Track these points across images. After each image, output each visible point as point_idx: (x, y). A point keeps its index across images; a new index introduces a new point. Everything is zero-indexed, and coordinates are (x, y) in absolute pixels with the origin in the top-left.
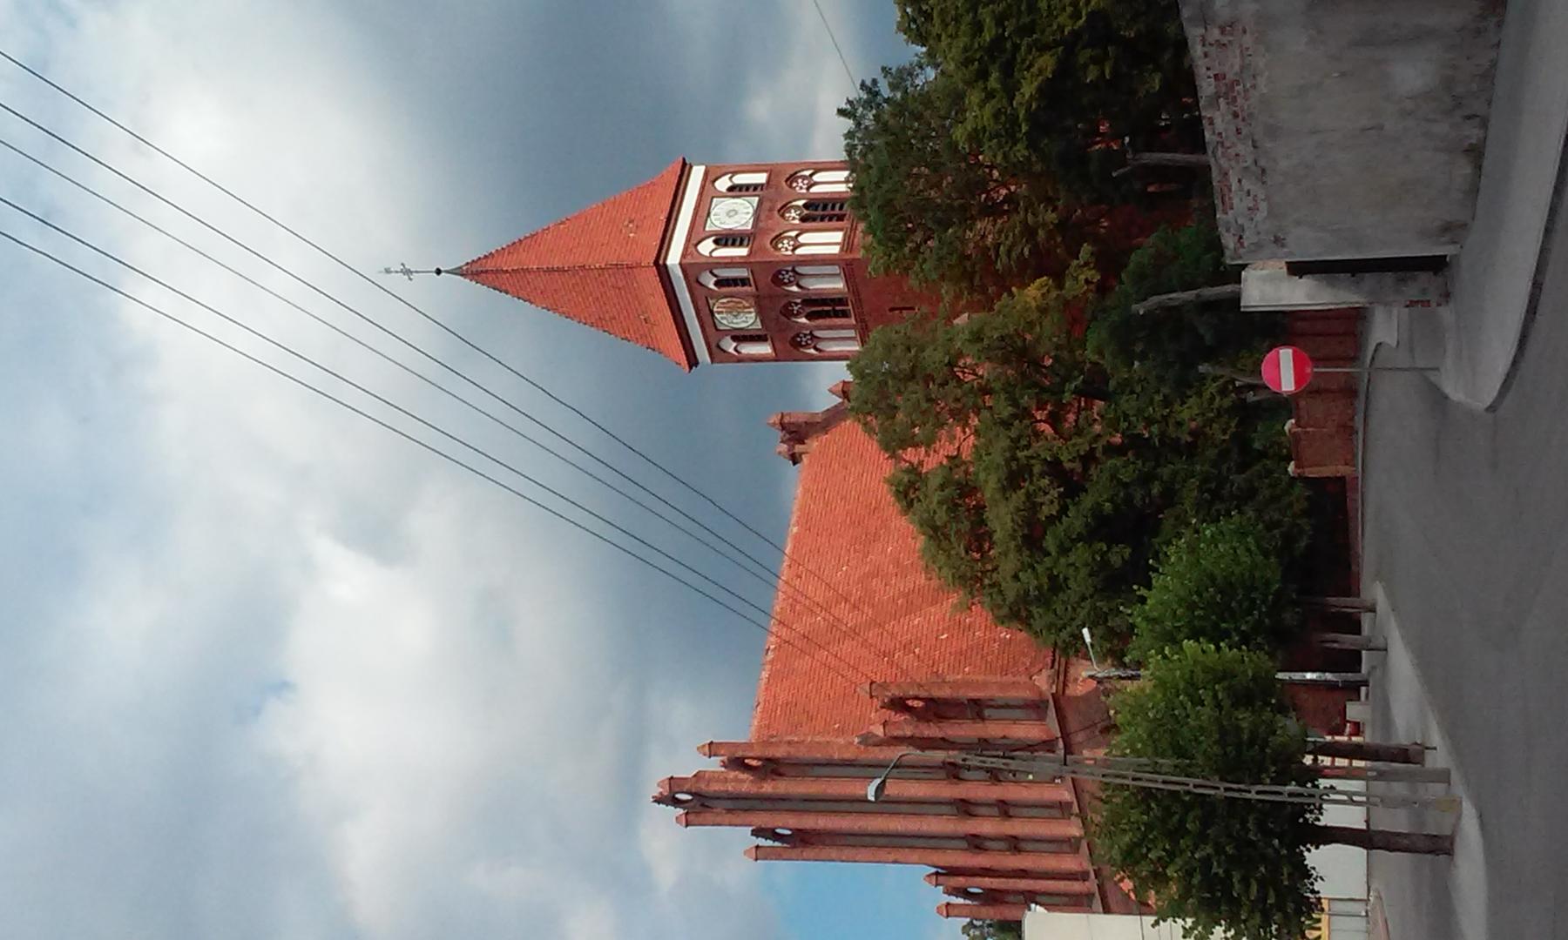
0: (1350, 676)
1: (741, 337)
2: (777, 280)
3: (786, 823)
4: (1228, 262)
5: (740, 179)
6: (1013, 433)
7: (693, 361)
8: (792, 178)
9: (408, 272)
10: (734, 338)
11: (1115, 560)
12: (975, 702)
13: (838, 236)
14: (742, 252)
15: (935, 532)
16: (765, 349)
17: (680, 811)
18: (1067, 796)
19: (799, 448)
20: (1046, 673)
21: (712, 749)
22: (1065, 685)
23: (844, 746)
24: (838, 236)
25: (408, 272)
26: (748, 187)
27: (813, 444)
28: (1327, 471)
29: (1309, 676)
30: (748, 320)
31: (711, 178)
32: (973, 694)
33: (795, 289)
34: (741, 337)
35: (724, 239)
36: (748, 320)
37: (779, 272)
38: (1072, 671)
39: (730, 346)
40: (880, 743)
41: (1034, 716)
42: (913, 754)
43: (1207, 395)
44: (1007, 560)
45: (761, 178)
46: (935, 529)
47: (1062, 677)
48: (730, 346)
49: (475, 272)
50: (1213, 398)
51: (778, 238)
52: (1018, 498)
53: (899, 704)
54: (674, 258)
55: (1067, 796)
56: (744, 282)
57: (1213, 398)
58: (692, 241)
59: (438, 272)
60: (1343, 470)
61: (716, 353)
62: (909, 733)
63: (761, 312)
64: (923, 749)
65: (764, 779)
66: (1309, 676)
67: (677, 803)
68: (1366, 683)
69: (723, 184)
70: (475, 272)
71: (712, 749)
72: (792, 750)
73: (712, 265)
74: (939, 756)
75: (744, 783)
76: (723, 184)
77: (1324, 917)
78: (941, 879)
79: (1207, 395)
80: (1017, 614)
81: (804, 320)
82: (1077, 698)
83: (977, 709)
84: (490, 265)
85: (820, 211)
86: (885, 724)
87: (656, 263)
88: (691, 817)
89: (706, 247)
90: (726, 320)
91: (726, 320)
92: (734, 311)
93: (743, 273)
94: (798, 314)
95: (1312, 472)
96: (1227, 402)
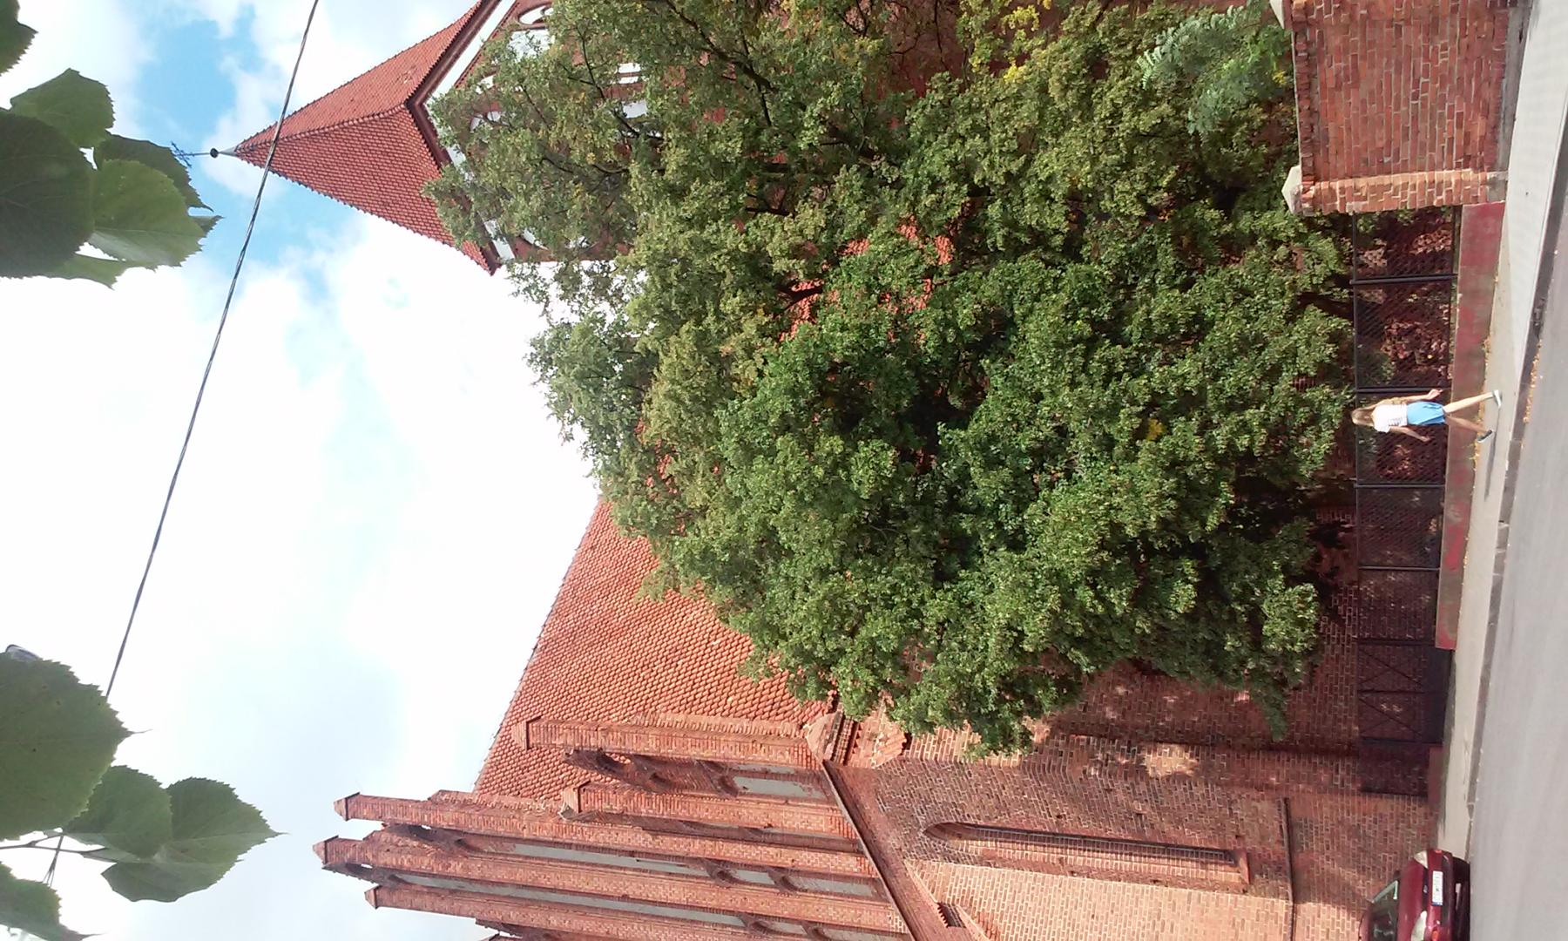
4: (1310, 587)
6: (689, 208)
11: (862, 479)
22: (851, 745)
28: (1405, 189)
31: (518, 10)
42: (642, 840)
43: (1102, 111)
50: (1116, 115)
57: (1116, 115)
60: (1450, 180)
62: (617, 808)
65: (451, 855)
74: (697, 847)
79: (1102, 111)
82: (868, 773)
83: (720, 778)
87: (409, 103)
88: (382, 894)
95: (1359, 194)
96: (1146, 121)
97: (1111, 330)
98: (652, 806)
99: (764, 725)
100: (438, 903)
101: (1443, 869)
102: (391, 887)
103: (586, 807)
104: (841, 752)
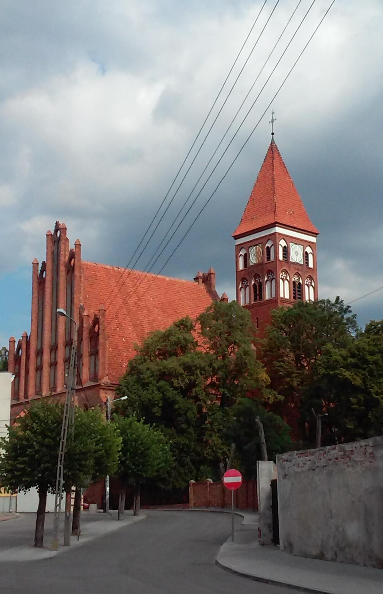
0: (108, 505)
1: (246, 257)
2: (269, 272)
3: (48, 275)
5: (310, 257)
6: (207, 368)
7: (236, 237)
8: (311, 278)
9: (272, 121)
10: (245, 254)
12: (97, 353)
13: (287, 297)
14: (281, 258)
15: (166, 336)
16: (241, 267)
17: (53, 232)
18: (59, 390)
19: (201, 280)
20: (109, 381)
21: (78, 245)
22: (104, 389)
23: (79, 299)
24: (287, 297)
25: (272, 121)
26: (307, 260)
27: (202, 287)
28: (191, 496)
29: (108, 488)
30: (253, 260)
32: (100, 352)
33: (266, 279)
34: (246, 257)
35: (286, 250)
36: (253, 260)
37: (273, 273)
38: (110, 392)
39: (242, 253)
40: (80, 314)
41: (92, 376)
43: (222, 447)
44: (155, 365)
45: (311, 265)
46: (168, 336)
47: (107, 388)
48: (242, 253)
49: (273, 149)
50: (221, 449)
51: (286, 272)
52: (181, 370)
53: (96, 321)
54: (278, 230)
55: (59, 390)
56: (269, 258)
57: (221, 449)
58: (285, 237)
59: (273, 134)
60: (192, 502)
61: (240, 247)
62: (84, 325)
63: (256, 265)
64: (78, 331)
66: (108, 488)
67: (56, 231)
68: (105, 512)
69: (308, 250)
70: (273, 149)
71: (78, 245)
72: (77, 278)
73: (275, 245)
74: (75, 338)
75: (64, 258)
76: (308, 250)
77: (9, 495)
78: (25, 338)
79: (222, 447)
80: (133, 369)
81: (253, 282)
82: (99, 394)
83: (94, 353)
84: (275, 155)
85: (297, 290)
86: (88, 316)
87: (276, 223)
88: (50, 237)
89: (283, 243)
90: (253, 251)
91: (253, 251)
92: (257, 255)
93: (272, 258)
94: (255, 280)
96: (219, 455)
97: (181, 451)
98: (85, 335)
99: (107, 366)
100: (49, 254)
101: (279, 260)
102: (141, 486)
103: (84, 317)
104: (103, 387)
